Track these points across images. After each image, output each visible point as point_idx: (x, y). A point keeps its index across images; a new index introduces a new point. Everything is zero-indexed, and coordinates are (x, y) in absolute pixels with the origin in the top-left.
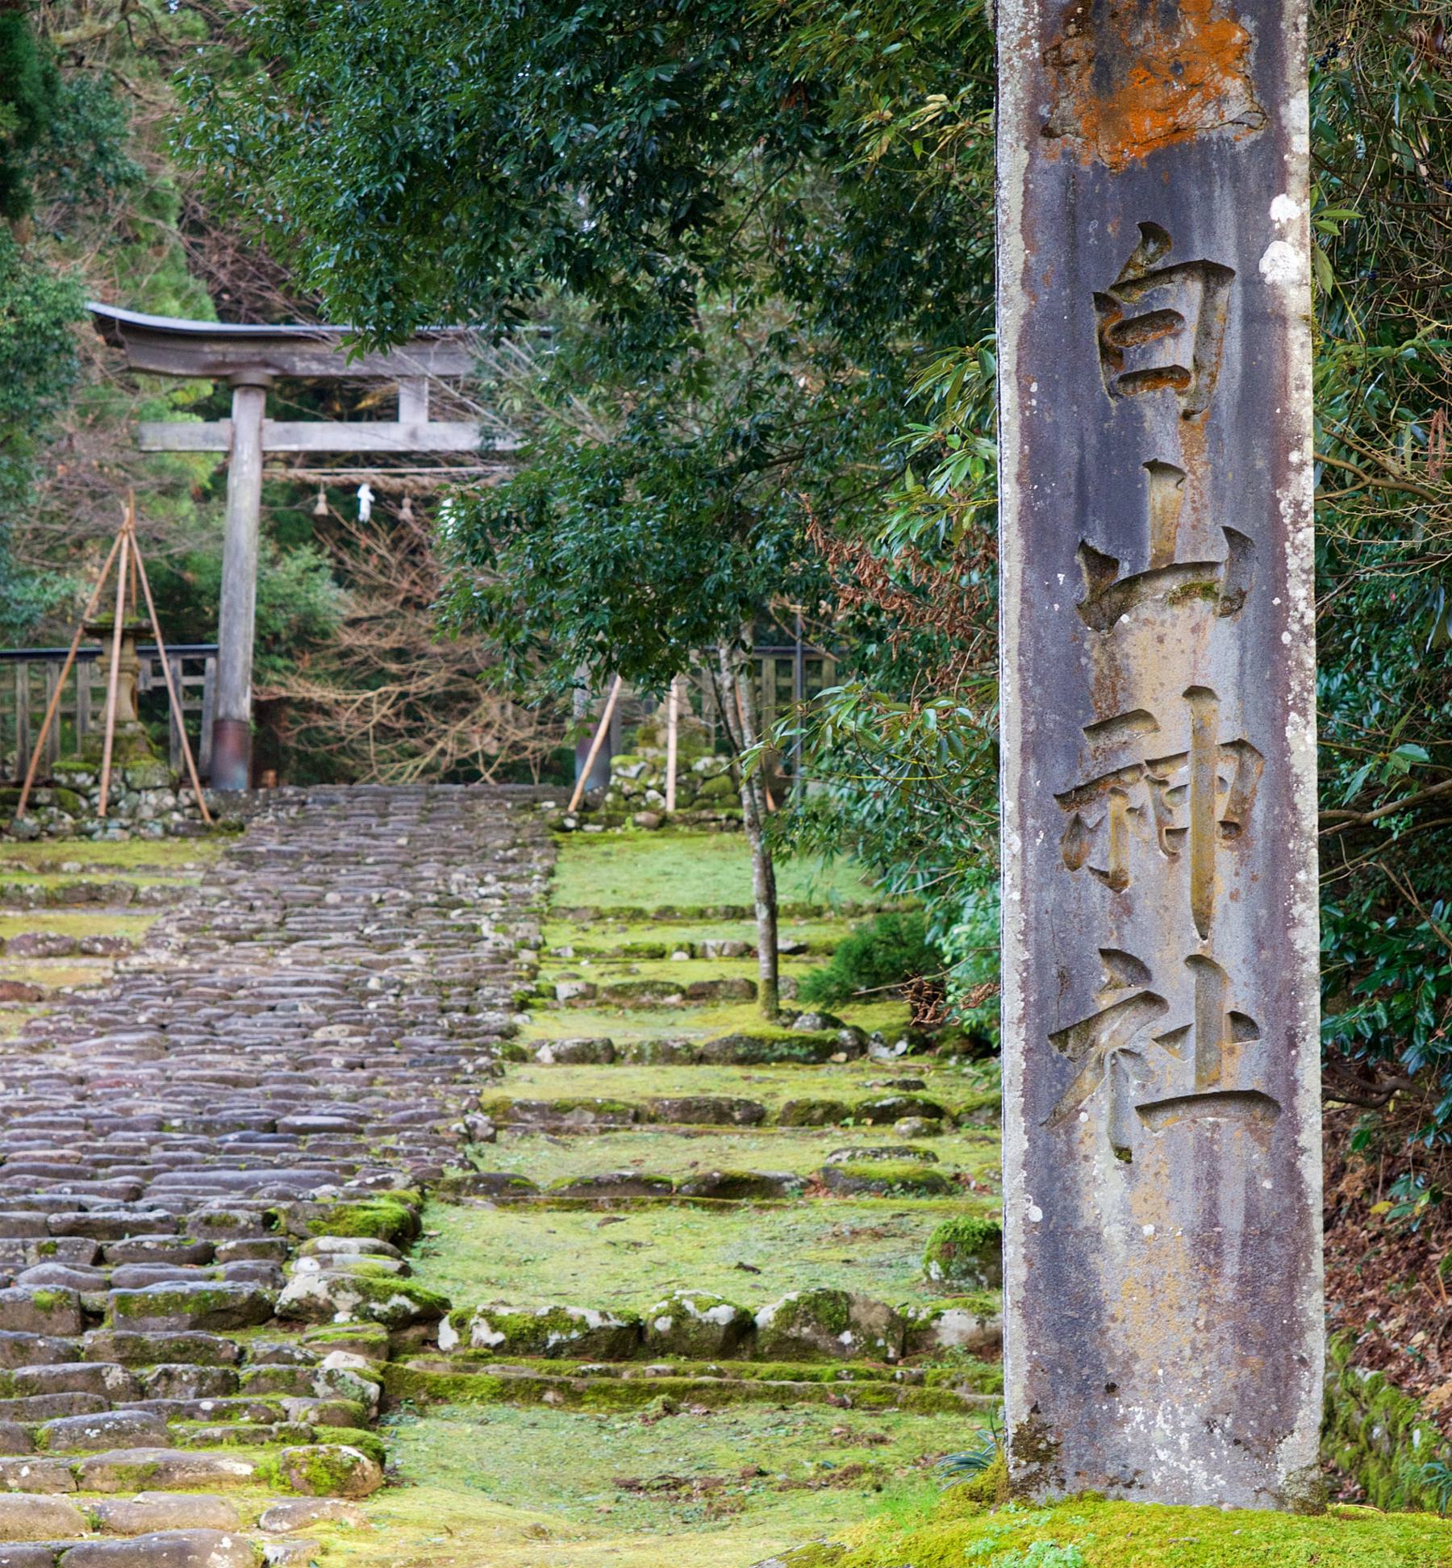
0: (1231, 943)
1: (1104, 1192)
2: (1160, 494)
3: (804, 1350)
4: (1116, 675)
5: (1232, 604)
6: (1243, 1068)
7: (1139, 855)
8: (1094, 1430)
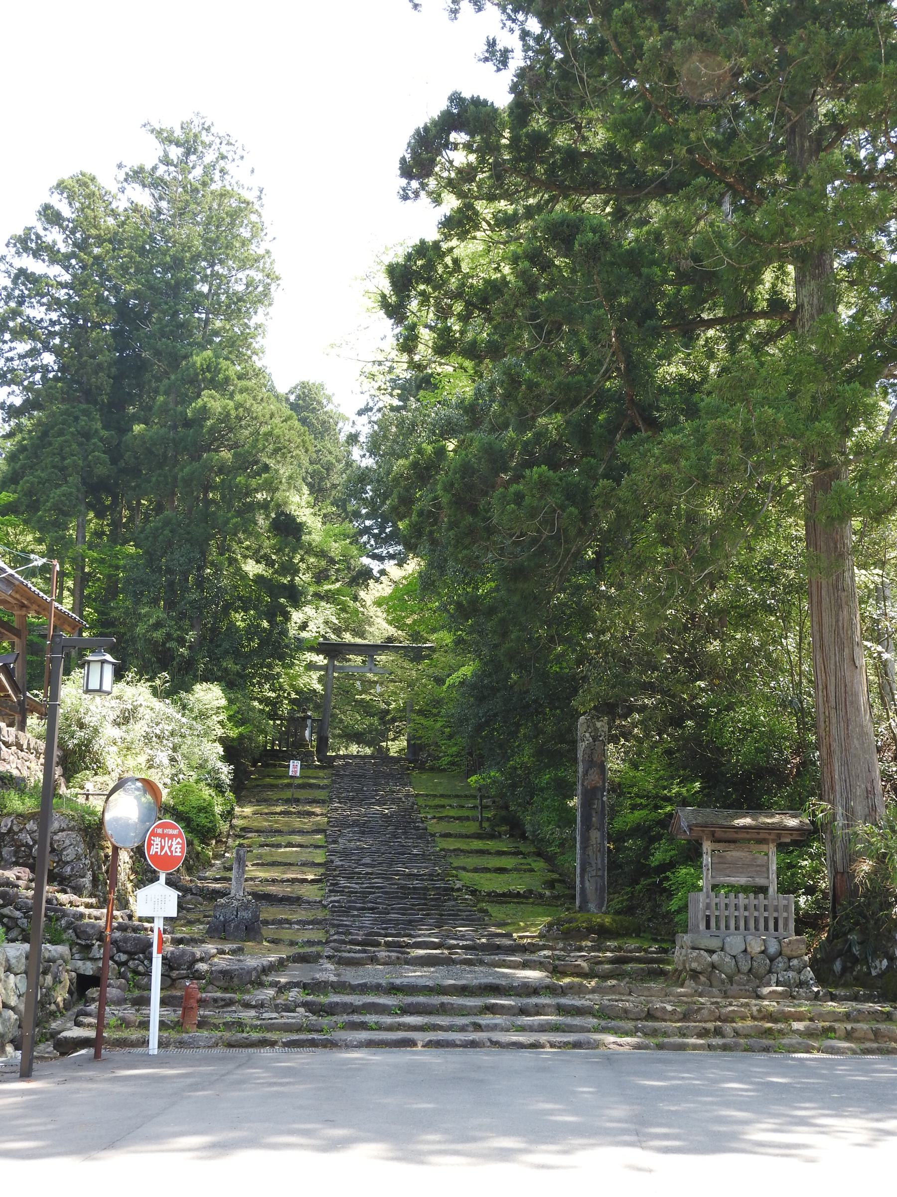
0: (599, 861)
1: (587, 884)
6: (600, 873)
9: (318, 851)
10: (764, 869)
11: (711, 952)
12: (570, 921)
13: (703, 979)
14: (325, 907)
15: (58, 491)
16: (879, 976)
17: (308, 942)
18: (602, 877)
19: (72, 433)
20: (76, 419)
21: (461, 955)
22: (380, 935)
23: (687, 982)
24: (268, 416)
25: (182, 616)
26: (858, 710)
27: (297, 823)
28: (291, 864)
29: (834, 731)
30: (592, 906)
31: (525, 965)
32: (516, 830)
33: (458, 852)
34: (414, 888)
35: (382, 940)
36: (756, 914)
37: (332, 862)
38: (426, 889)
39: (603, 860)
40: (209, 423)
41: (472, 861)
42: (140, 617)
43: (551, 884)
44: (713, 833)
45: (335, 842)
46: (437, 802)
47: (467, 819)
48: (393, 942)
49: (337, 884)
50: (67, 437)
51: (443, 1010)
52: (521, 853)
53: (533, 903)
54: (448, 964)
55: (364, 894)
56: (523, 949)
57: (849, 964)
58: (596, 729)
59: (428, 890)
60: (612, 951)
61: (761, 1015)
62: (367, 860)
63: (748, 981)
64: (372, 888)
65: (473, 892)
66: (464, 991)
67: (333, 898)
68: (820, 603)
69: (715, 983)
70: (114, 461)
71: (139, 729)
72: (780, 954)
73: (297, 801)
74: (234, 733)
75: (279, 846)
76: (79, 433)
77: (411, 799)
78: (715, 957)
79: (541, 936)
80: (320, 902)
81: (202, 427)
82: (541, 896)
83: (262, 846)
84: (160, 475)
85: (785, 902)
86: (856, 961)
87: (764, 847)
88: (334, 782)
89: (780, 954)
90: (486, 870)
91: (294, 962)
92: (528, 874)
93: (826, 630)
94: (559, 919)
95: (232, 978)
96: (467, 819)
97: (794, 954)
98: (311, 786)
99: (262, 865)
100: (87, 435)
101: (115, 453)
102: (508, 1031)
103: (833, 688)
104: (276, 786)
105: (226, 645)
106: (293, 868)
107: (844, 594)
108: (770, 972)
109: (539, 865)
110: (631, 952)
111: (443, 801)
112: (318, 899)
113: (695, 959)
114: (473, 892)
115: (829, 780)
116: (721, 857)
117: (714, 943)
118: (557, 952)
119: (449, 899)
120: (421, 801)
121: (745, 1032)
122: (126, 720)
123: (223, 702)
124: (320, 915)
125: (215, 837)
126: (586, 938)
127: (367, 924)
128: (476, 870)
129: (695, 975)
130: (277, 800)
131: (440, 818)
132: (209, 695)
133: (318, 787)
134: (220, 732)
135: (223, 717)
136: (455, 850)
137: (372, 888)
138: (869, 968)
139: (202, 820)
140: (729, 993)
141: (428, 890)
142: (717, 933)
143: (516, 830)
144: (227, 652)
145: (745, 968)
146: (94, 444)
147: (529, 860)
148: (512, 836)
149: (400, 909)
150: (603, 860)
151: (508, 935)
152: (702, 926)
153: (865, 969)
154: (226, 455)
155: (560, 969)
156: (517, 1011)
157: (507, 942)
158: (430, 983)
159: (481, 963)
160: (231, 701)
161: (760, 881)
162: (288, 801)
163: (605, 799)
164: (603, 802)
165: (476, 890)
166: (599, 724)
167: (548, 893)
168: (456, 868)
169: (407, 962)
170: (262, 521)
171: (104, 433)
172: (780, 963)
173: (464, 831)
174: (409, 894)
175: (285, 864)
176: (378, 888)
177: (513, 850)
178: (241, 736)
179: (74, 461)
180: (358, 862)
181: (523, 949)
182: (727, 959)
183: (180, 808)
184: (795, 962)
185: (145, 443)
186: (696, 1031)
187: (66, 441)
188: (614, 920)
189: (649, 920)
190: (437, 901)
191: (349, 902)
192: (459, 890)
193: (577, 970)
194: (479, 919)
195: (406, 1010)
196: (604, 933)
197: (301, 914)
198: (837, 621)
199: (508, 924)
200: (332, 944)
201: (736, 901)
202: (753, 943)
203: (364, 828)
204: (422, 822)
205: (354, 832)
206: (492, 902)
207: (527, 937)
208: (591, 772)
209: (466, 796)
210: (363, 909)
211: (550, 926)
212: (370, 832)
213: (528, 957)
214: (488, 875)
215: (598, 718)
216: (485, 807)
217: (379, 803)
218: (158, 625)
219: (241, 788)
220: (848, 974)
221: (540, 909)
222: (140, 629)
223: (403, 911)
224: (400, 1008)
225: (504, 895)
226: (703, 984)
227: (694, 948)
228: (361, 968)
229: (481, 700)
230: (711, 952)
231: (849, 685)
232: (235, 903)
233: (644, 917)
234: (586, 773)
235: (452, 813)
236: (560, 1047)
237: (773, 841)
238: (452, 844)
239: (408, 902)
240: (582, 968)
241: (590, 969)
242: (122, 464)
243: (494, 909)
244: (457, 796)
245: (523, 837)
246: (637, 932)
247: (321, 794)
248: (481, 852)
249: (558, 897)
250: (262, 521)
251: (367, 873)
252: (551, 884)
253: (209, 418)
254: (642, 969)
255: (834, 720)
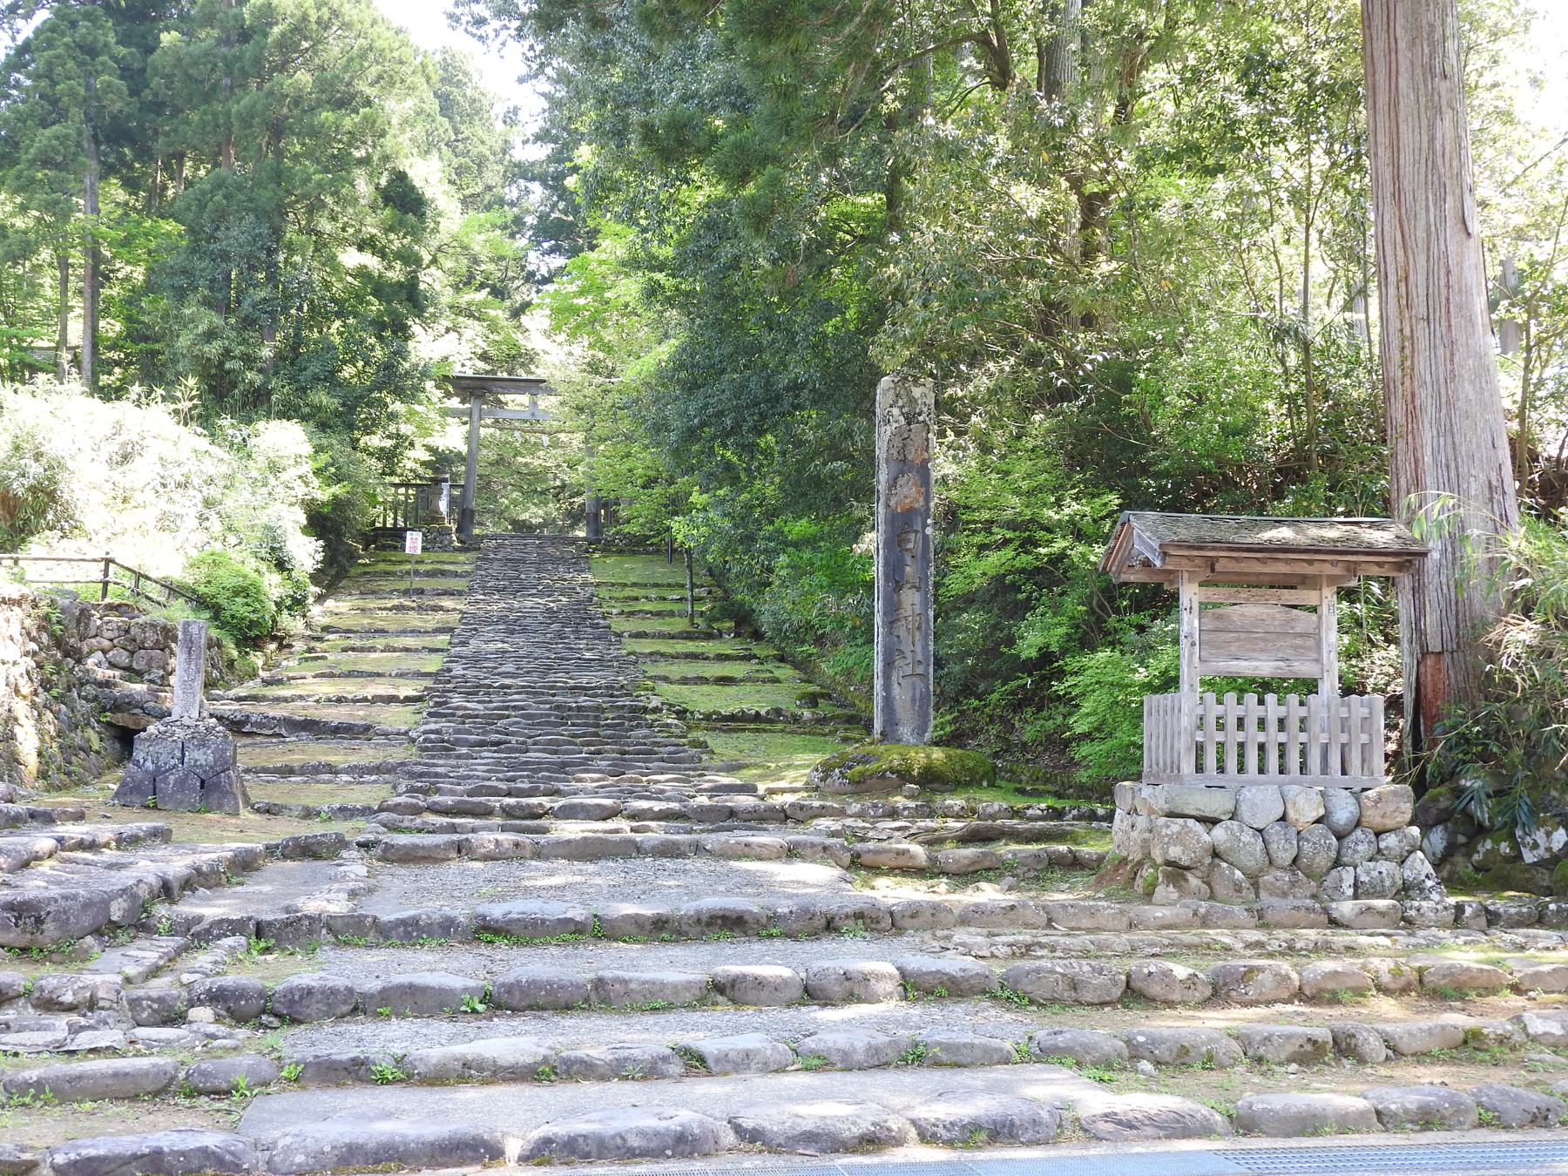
0: (918, 648)
1: (896, 690)
2: (908, 569)
3: (771, 722)
4: (899, 602)
5: (918, 589)
6: (920, 670)
7: (902, 633)
8: (894, 731)
9: (433, 655)
10: (1311, 642)
11: (1211, 822)
12: (865, 760)
13: (1194, 881)
14: (413, 741)
15: (48, 132)
16: (1541, 863)
17: (342, 809)
18: (924, 676)
19: (66, 45)
20: (73, 25)
21: (657, 833)
22: (495, 792)
23: (1161, 891)
24: (367, 25)
25: (248, 322)
26: (1471, 321)
27: (414, 620)
28: (379, 675)
29: (1422, 365)
30: (905, 731)
31: (791, 853)
32: (745, 623)
33: (656, 656)
34: (579, 708)
35: (495, 802)
36: (1220, 737)
37: (449, 670)
38: (598, 708)
39: (925, 646)
40: (276, 30)
41: (677, 670)
42: (186, 323)
43: (812, 700)
44: (1211, 564)
45: (464, 644)
46: (628, 592)
47: (672, 614)
48: (519, 807)
49: (445, 703)
50: (60, 51)
51: (601, 997)
52: (755, 657)
53: (782, 731)
54: (626, 856)
55: (491, 719)
56: (783, 816)
57: (1462, 839)
58: (912, 401)
59: (604, 710)
60: (958, 817)
61: (1401, 982)
62: (509, 668)
63: (1293, 884)
64: (507, 708)
65: (681, 714)
66: (660, 929)
67: (432, 726)
68: (1394, 104)
69: (1220, 890)
70: (134, 92)
71: (142, 471)
72: (1358, 824)
73: (421, 592)
74: (323, 494)
75: (372, 649)
76: (78, 46)
77: (590, 590)
78: (1219, 833)
79: (811, 788)
80: (406, 733)
81: (266, 35)
82: (796, 719)
83: (345, 650)
84: (205, 113)
85: (1365, 711)
86: (1480, 831)
87: (1308, 596)
88: (478, 568)
89: (1358, 824)
90: (702, 680)
91: (285, 857)
92: (769, 686)
93: (1406, 160)
94: (842, 756)
95: (39, 921)
96: (672, 614)
97: (1389, 823)
98: (443, 573)
99: (332, 675)
100: (91, 51)
101: (134, 77)
102: (781, 1070)
103: (1422, 279)
104: (393, 574)
105: (314, 368)
106: (378, 680)
107: (1444, 86)
108: (1337, 863)
109: (785, 672)
110: (993, 817)
111: (636, 592)
112: (403, 728)
113: (1177, 839)
114: (681, 714)
115: (1410, 468)
116: (1220, 617)
117: (1215, 804)
118: (849, 822)
119: (638, 726)
120: (604, 592)
121: (1417, 1046)
122: (126, 458)
123: (308, 449)
124: (397, 754)
125: (274, 638)
126: (897, 789)
127: (480, 771)
128: (684, 681)
129: (1177, 871)
130: (391, 592)
131: (632, 613)
132: (284, 439)
133: (456, 575)
134: (300, 490)
135: (307, 468)
136: (651, 654)
137: (507, 708)
138: (1516, 846)
139: (239, 608)
140: (1269, 916)
141: (604, 710)
142: (1220, 779)
143: (745, 623)
144: (316, 378)
145: (1284, 856)
146: (103, 64)
147: (769, 666)
148: (738, 635)
149: (550, 742)
150: (925, 646)
151: (748, 789)
152: (1188, 766)
153: (1505, 848)
154: (304, 78)
155: (866, 859)
156: (797, 992)
157: (744, 801)
158: (577, 913)
159: (698, 849)
160: (319, 450)
161: (1305, 669)
162: (406, 593)
163: (929, 531)
164: (926, 537)
165: (686, 711)
166: (917, 392)
167: (807, 714)
168: (650, 678)
169: (539, 854)
170: (363, 187)
171: (122, 51)
172: (1361, 844)
173: (666, 629)
174: (570, 717)
175: (371, 675)
176: (515, 708)
177: (743, 653)
178: (336, 502)
179: (71, 88)
180: (492, 671)
181: (783, 816)
182: (1248, 836)
183: (202, 589)
184: (1390, 841)
185: (180, 60)
186: (1290, 1048)
187: (57, 57)
188: (949, 757)
189: (996, 755)
190: (618, 730)
191: (458, 732)
192: (656, 710)
193: (901, 861)
194: (691, 759)
195: (502, 1002)
196: (932, 780)
197: (367, 755)
198: (1432, 140)
199: (746, 766)
200: (383, 816)
201: (1282, 711)
202: (1301, 800)
203: (513, 626)
204: (604, 618)
205: (499, 631)
206: (714, 729)
207: (783, 791)
208: (902, 481)
209: (669, 585)
210: (482, 744)
211: (827, 769)
212: (524, 630)
213: (792, 835)
214: (705, 688)
215: (916, 380)
216: (695, 599)
217: (541, 594)
218: (210, 335)
219: (335, 573)
220: (1459, 859)
221: (797, 740)
222: (184, 342)
223: (553, 747)
224: (487, 998)
225: (732, 718)
226: (1196, 894)
227: (1171, 815)
228: (432, 870)
229: (691, 387)
230: (1211, 822)
231: (1454, 270)
232: (180, 733)
233: (988, 751)
234: (893, 484)
235: (649, 607)
236: (950, 1143)
237: (1332, 580)
238: (646, 646)
239: (564, 732)
240: (912, 857)
241: (930, 859)
242: (147, 95)
243: (716, 741)
244: (656, 585)
245: (757, 636)
246: (989, 778)
247: (459, 584)
248: (694, 657)
249: (822, 721)
250: (363, 187)
251: (503, 687)
252: (812, 700)
253: (277, 23)
254: (1037, 856)
255: (1422, 344)
